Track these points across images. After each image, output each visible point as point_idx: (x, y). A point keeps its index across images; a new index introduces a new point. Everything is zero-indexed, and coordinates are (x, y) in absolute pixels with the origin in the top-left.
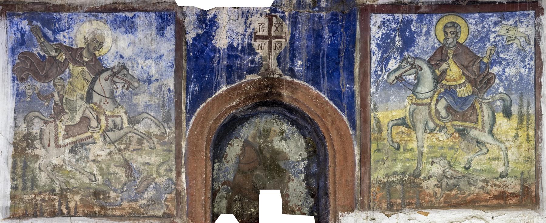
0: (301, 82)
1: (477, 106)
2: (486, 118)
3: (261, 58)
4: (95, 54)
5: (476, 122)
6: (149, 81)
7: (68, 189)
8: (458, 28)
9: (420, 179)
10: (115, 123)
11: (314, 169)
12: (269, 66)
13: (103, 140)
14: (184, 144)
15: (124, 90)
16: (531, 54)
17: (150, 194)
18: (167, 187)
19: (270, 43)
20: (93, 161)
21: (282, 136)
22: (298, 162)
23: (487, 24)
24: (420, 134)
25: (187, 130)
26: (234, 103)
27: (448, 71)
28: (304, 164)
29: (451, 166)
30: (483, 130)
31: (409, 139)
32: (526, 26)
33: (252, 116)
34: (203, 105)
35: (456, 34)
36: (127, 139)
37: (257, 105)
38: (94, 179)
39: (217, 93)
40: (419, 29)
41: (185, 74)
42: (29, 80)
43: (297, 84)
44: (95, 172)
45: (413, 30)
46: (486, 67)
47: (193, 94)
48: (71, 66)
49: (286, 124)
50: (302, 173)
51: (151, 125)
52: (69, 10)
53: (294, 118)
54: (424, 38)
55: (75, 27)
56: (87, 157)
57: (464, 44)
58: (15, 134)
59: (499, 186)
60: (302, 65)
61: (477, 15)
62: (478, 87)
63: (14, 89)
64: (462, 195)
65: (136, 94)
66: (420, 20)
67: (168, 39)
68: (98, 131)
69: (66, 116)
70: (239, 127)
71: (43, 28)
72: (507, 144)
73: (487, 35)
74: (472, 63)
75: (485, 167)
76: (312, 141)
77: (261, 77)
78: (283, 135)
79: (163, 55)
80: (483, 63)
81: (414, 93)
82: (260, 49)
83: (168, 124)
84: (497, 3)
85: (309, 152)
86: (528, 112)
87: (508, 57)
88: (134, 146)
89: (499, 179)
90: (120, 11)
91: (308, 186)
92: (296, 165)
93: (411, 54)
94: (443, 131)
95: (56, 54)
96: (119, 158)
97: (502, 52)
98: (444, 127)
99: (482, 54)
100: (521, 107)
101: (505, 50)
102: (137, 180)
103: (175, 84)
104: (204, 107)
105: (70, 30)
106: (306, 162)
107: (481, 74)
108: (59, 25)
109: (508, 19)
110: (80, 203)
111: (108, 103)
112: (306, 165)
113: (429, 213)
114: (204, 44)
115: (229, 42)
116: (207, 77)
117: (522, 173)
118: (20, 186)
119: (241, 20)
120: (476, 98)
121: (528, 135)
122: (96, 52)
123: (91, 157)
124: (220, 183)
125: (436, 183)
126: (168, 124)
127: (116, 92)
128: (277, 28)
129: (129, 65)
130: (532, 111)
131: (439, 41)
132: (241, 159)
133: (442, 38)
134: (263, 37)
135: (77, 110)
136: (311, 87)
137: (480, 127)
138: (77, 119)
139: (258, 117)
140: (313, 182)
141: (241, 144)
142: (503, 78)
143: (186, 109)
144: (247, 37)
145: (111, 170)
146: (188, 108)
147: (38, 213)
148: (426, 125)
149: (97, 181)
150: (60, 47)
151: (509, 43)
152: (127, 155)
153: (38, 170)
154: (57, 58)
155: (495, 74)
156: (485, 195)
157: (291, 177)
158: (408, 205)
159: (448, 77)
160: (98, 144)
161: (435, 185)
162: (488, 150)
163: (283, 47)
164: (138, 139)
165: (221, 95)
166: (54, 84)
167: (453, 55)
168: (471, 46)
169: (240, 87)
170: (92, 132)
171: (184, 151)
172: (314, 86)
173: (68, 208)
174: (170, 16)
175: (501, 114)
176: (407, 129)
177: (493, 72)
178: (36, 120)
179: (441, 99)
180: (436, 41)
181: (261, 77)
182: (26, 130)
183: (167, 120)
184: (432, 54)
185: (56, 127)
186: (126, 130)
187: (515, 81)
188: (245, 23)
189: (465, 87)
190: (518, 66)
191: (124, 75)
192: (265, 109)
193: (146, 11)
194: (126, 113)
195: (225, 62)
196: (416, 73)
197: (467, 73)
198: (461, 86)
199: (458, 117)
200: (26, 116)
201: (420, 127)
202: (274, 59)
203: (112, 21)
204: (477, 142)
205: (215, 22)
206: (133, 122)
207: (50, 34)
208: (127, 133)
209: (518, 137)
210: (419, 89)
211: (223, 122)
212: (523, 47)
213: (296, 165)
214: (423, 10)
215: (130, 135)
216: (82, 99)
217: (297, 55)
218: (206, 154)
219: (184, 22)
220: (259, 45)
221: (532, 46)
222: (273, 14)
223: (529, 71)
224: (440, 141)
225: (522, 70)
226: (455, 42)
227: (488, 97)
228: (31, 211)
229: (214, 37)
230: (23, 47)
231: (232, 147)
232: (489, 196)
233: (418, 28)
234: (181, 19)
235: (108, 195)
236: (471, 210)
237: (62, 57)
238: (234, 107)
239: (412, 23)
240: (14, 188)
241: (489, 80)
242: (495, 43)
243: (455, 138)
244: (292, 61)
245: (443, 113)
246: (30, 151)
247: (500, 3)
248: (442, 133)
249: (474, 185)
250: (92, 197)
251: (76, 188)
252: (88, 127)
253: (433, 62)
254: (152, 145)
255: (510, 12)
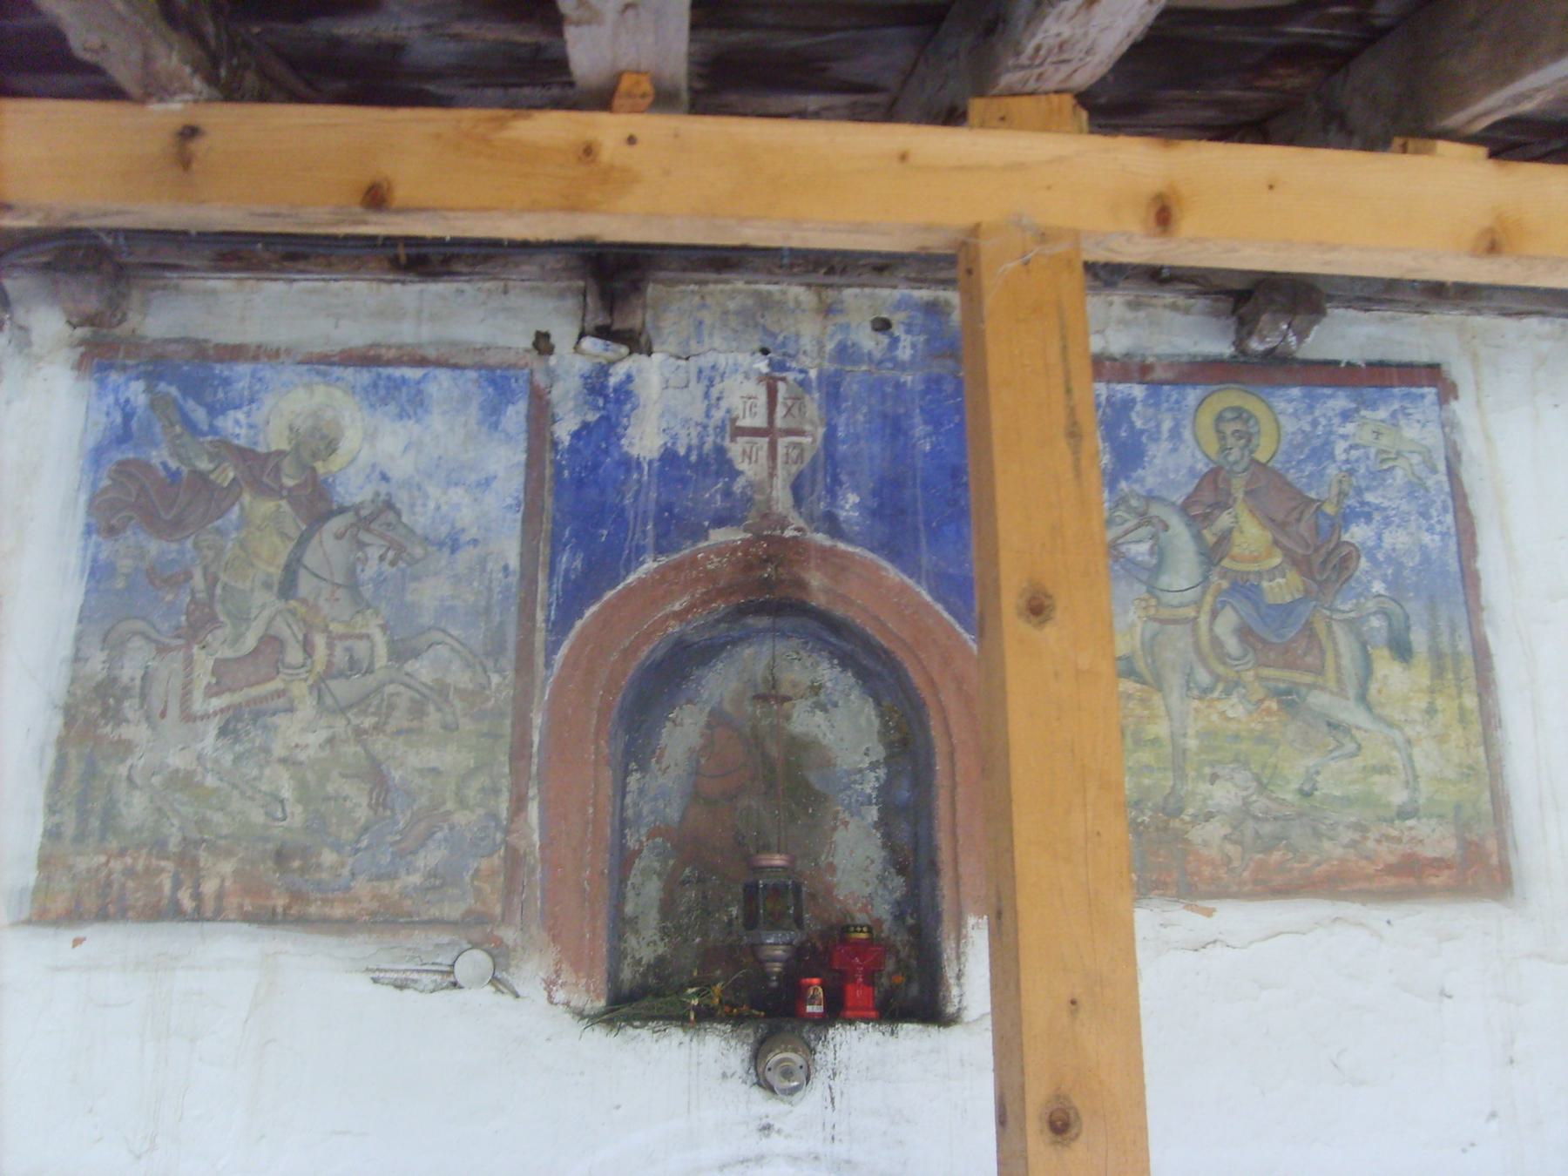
0: (858, 550)
1: (1320, 627)
2: (1346, 661)
3: (750, 484)
4: (314, 470)
5: (1319, 671)
6: (453, 544)
7: (204, 841)
8: (1252, 422)
9: (1182, 820)
10: (351, 657)
11: (903, 793)
12: (770, 508)
13: (314, 703)
14: (538, 720)
15: (386, 566)
16: (1443, 497)
17: (432, 857)
18: (482, 839)
19: (773, 447)
20: (283, 761)
21: (815, 699)
22: (861, 771)
23: (1324, 415)
24: (1175, 699)
25: (547, 679)
26: (677, 607)
27: (1236, 534)
28: (877, 779)
29: (1262, 787)
30: (1341, 692)
31: (1146, 713)
32: (1419, 426)
33: (735, 642)
34: (594, 609)
35: (1248, 438)
36: (382, 700)
37: (741, 612)
38: (279, 814)
39: (631, 578)
40: (1152, 424)
41: (547, 526)
42: (129, 533)
43: (844, 555)
44: (286, 793)
45: (1139, 424)
46: (1332, 526)
47: (566, 579)
48: (247, 498)
49: (826, 664)
50: (870, 803)
51: (451, 662)
52: (256, 358)
53: (848, 647)
54: (1166, 445)
55: (269, 401)
56: (266, 750)
57: (1270, 465)
58: (73, 681)
59: (1399, 840)
60: (856, 506)
61: (1296, 392)
62: (1318, 578)
63: (85, 557)
64: (1300, 862)
65: (416, 578)
66: (1154, 400)
67: (509, 438)
68: (304, 676)
69: (218, 632)
70: (697, 673)
71: (184, 399)
72: (1410, 731)
73: (1327, 443)
74: (1295, 514)
75: (1354, 790)
76: (896, 712)
77: (749, 535)
78: (817, 694)
79: (495, 477)
80: (1326, 515)
81: (1152, 590)
82: (747, 461)
83: (496, 661)
84: (1343, 365)
85: (889, 745)
86: (1454, 646)
87: (1386, 504)
88: (399, 719)
89: (1397, 822)
90: (389, 363)
91: (889, 842)
92: (855, 782)
93: (1136, 487)
94: (1234, 692)
95: (211, 466)
96: (355, 753)
97: (1368, 489)
98: (1237, 684)
99: (1318, 494)
100: (1434, 634)
101: (1375, 483)
102: (400, 816)
103: (522, 555)
104: (596, 616)
105: (254, 406)
106: (882, 772)
107: (1322, 545)
108: (226, 393)
109: (1373, 406)
110: (235, 882)
111: (337, 600)
112: (882, 781)
113: (1214, 910)
114: (599, 447)
115: (665, 444)
116: (605, 532)
117: (1458, 807)
118: (70, 830)
119: (697, 389)
120: (1315, 607)
121: (1461, 708)
122: (319, 465)
123: (278, 750)
124: (644, 831)
125: (1227, 830)
126: (496, 661)
127: (363, 571)
128: (789, 409)
129: (402, 500)
130: (1464, 645)
131: (1207, 456)
132: (703, 761)
133: (1213, 448)
134: (755, 432)
135: (252, 616)
136: (884, 563)
137: (1332, 684)
138: (250, 641)
139: (750, 645)
140: (903, 831)
141: (703, 719)
142: (1380, 557)
143: (547, 620)
144: (711, 430)
145: (330, 788)
146: (553, 618)
147: (111, 909)
148: (1189, 677)
149: (288, 820)
150: (226, 449)
151: (1385, 466)
152: (378, 745)
153: (124, 784)
154: (212, 477)
155: (1357, 545)
156: (1363, 863)
157: (841, 816)
158: (1157, 888)
159: (1236, 551)
160: (299, 715)
161: (1226, 837)
162: (1359, 747)
163: (808, 456)
164: (413, 700)
165: (641, 581)
166: (196, 546)
167: (1246, 493)
168: (1288, 470)
169: (693, 562)
170: (288, 678)
171: (536, 738)
172: (892, 561)
173: (197, 896)
174: (517, 380)
175: (1385, 652)
176: (1138, 686)
177: (1353, 541)
178: (137, 642)
179: (1223, 608)
180: (1199, 455)
181: (749, 535)
182: (103, 669)
183: (495, 649)
184: (1190, 488)
185: (189, 662)
186: (380, 675)
187: (1411, 564)
188: (707, 395)
189: (1284, 576)
190: (1412, 527)
191: (389, 525)
192: (764, 622)
193: (455, 367)
194: (384, 628)
195: (653, 495)
196: (1154, 537)
197: (1284, 540)
198: (1272, 573)
199: (1272, 655)
200: (109, 631)
201: (1174, 680)
202: (784, 488)
203: (365, 390)
204: (1329, 724)
205: (629, 394)
206: (402, 652)
207: (200, 415)
208: (384, 685)
209: (1436, 711)
210: (1165, 581)
211: (648, 658)
212: (1420, 479)
213: (855, 782)
214: (1159, 374)
215: (390, 689)
216: (267, 586)
217: (844, 478)
218: (597, 748)
219: (550, 392)
220: (744, 452)
221: (1442, 477)
222: (777, 374)
223: (1442, 540)
224: (1230, 719)
225: (1426, 538)
226: (1246, 460)
227: (1346, 606)
228: (91, 903)
229: (626, 428)
230: (123, 447)
231: (679, 728)
232: (1374, 867)
233: (1151, 420)
234: (543, 385)
235: (314, 860)
236: (1328, 902)
237: (228, 474)
238: (678, 616)
239: (1132, 408)
240: (53, 834)
241: (1345, 560)
242: (1349, 466)
243: (1269, 712)
244: (832, 492)
245: (1232, 645)
246: (108, 729)
247: (1349, 364)
248: (1234, 699)
249: (1331, 839)
250: (270, 864)
251: (226, 837)
252: (277, 666)
253: (1196, 511)
254: (450, 718)
255: (1376, 387)
